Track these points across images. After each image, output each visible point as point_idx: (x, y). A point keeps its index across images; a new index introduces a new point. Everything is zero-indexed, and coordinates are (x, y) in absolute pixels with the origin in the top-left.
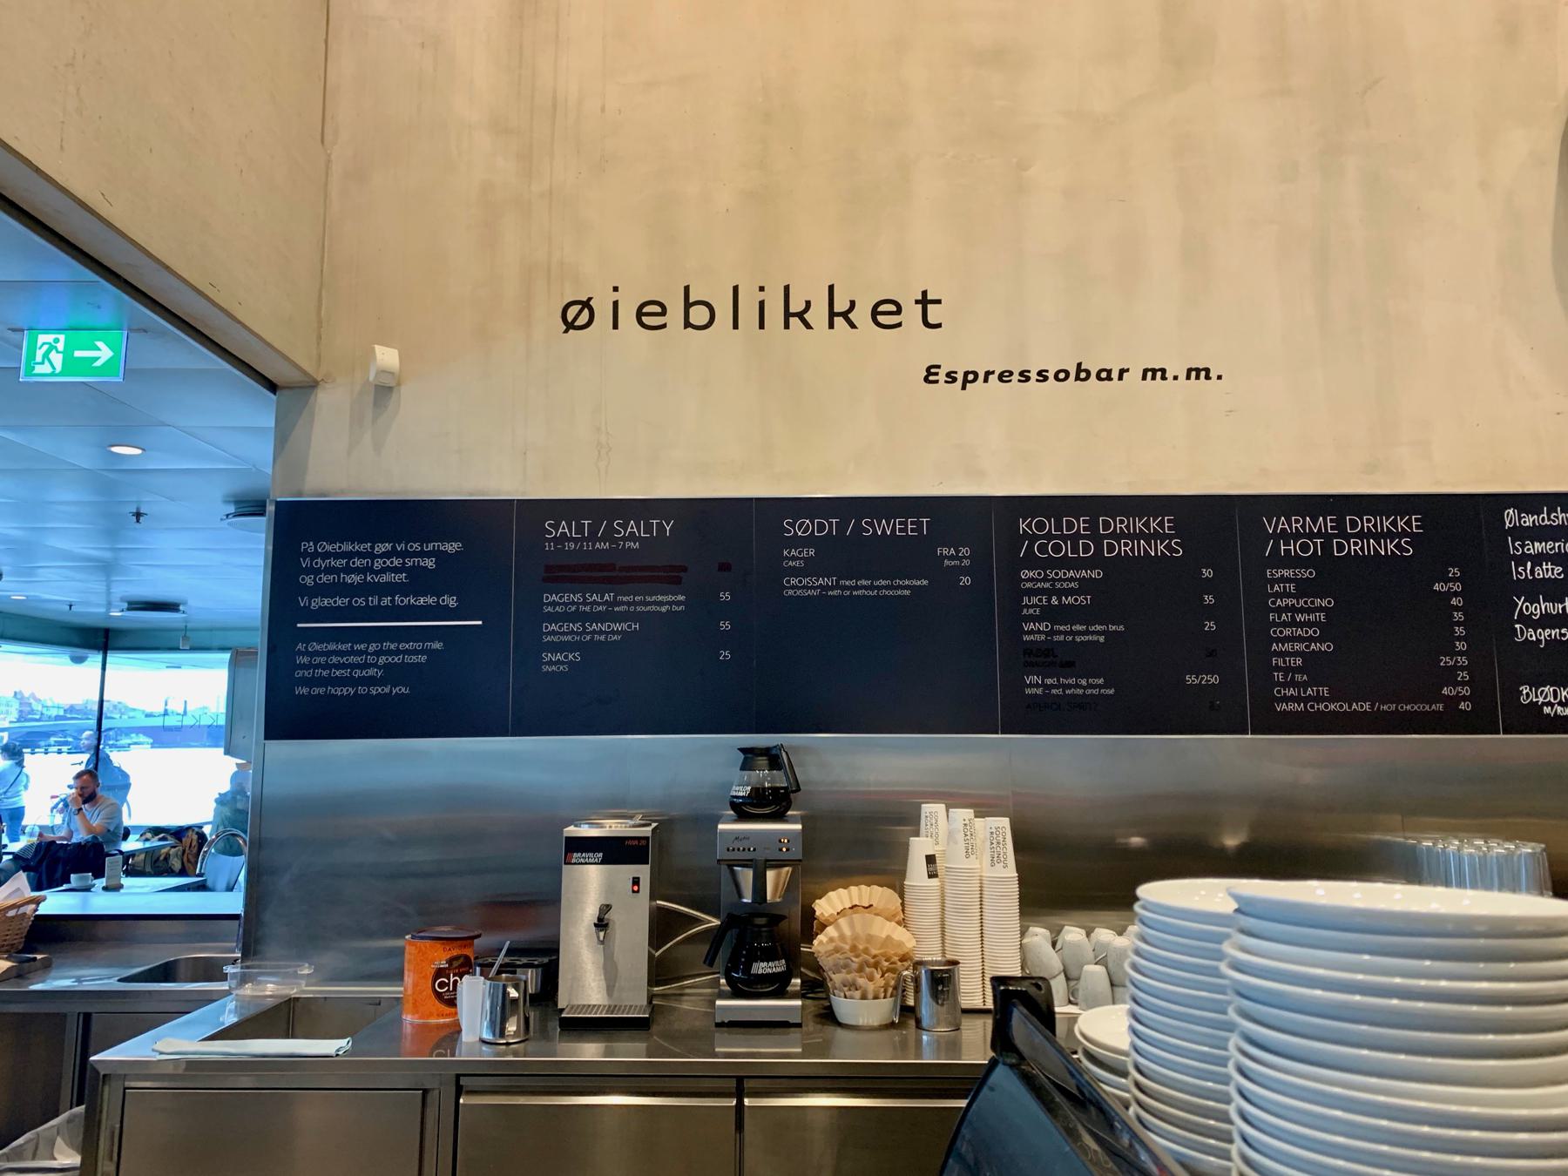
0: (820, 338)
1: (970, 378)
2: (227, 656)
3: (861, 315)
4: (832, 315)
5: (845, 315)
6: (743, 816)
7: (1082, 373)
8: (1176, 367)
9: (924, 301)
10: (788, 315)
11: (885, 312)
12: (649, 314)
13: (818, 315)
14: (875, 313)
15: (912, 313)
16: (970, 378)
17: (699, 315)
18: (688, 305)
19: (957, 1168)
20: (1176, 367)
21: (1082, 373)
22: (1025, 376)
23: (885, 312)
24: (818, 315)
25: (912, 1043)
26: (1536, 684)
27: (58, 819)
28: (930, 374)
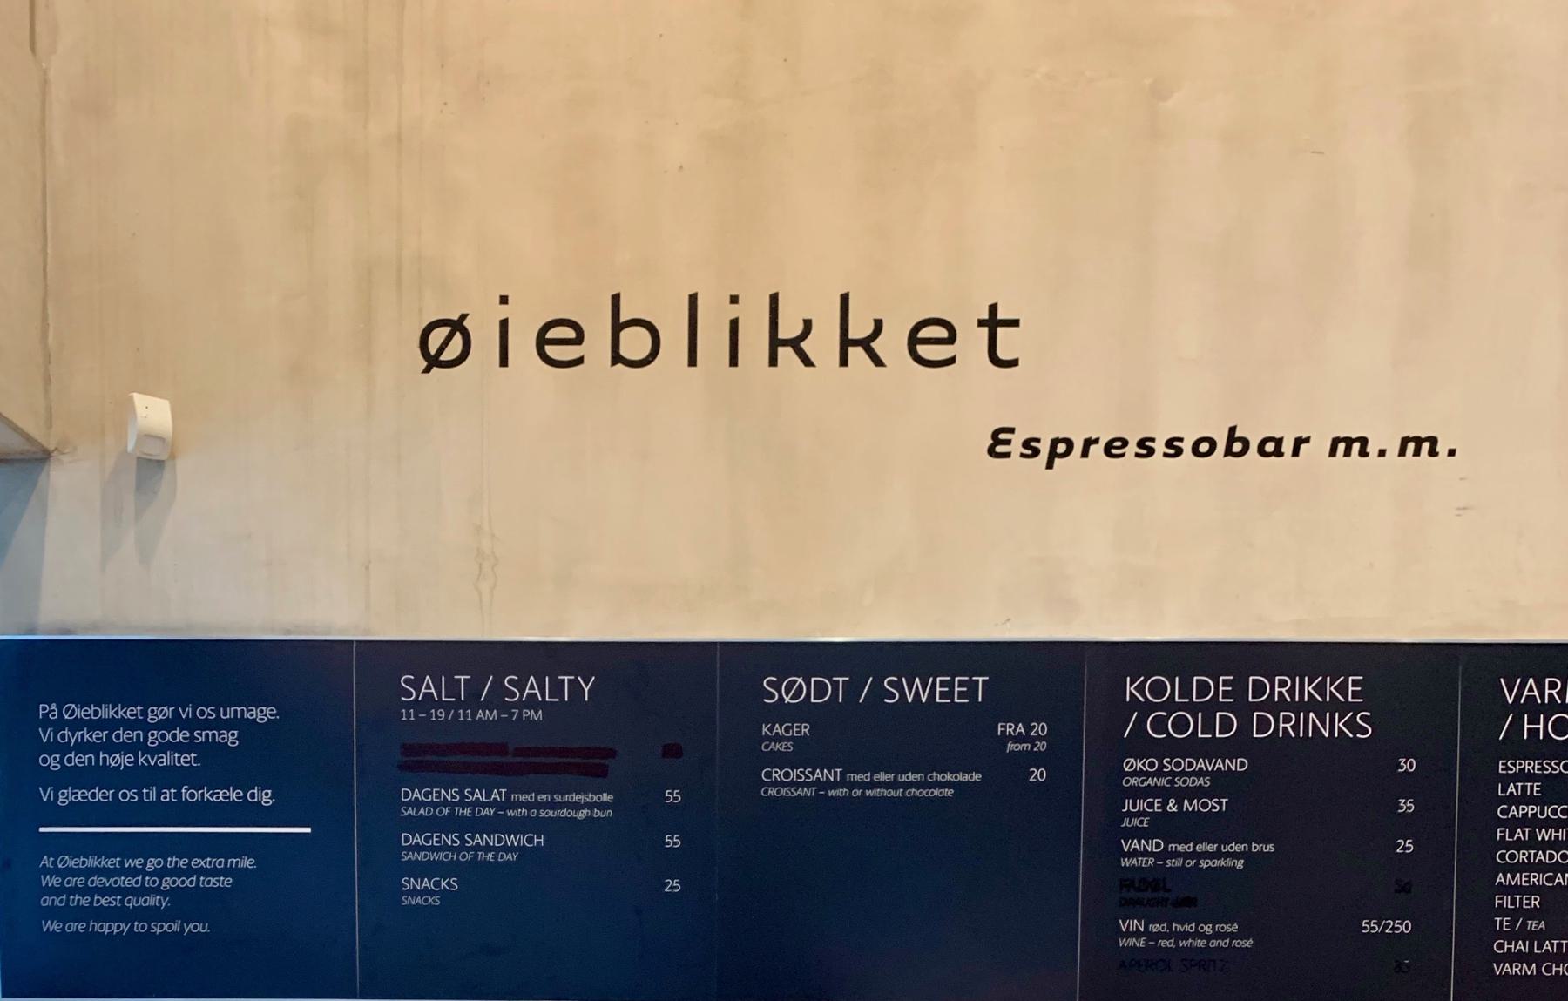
0: (824, 387)
1: (1060, 449)
3: (892, 344)
4: (846, 343)
5: (866, 344)
8: (1384, 436)
9: (992, 322)
10: (775, 342)
11: (929, 340)
12: (557, 340)
13: (823, 344)
14: (914, 341)
15: (973, 340)
16: (1060, 449)
17: (635, 343)
18: (618, 327)
20: (1384, 436)
21: (1235, 445)
23: (929, 340)
24: (823, 344)
28: (998, 443)
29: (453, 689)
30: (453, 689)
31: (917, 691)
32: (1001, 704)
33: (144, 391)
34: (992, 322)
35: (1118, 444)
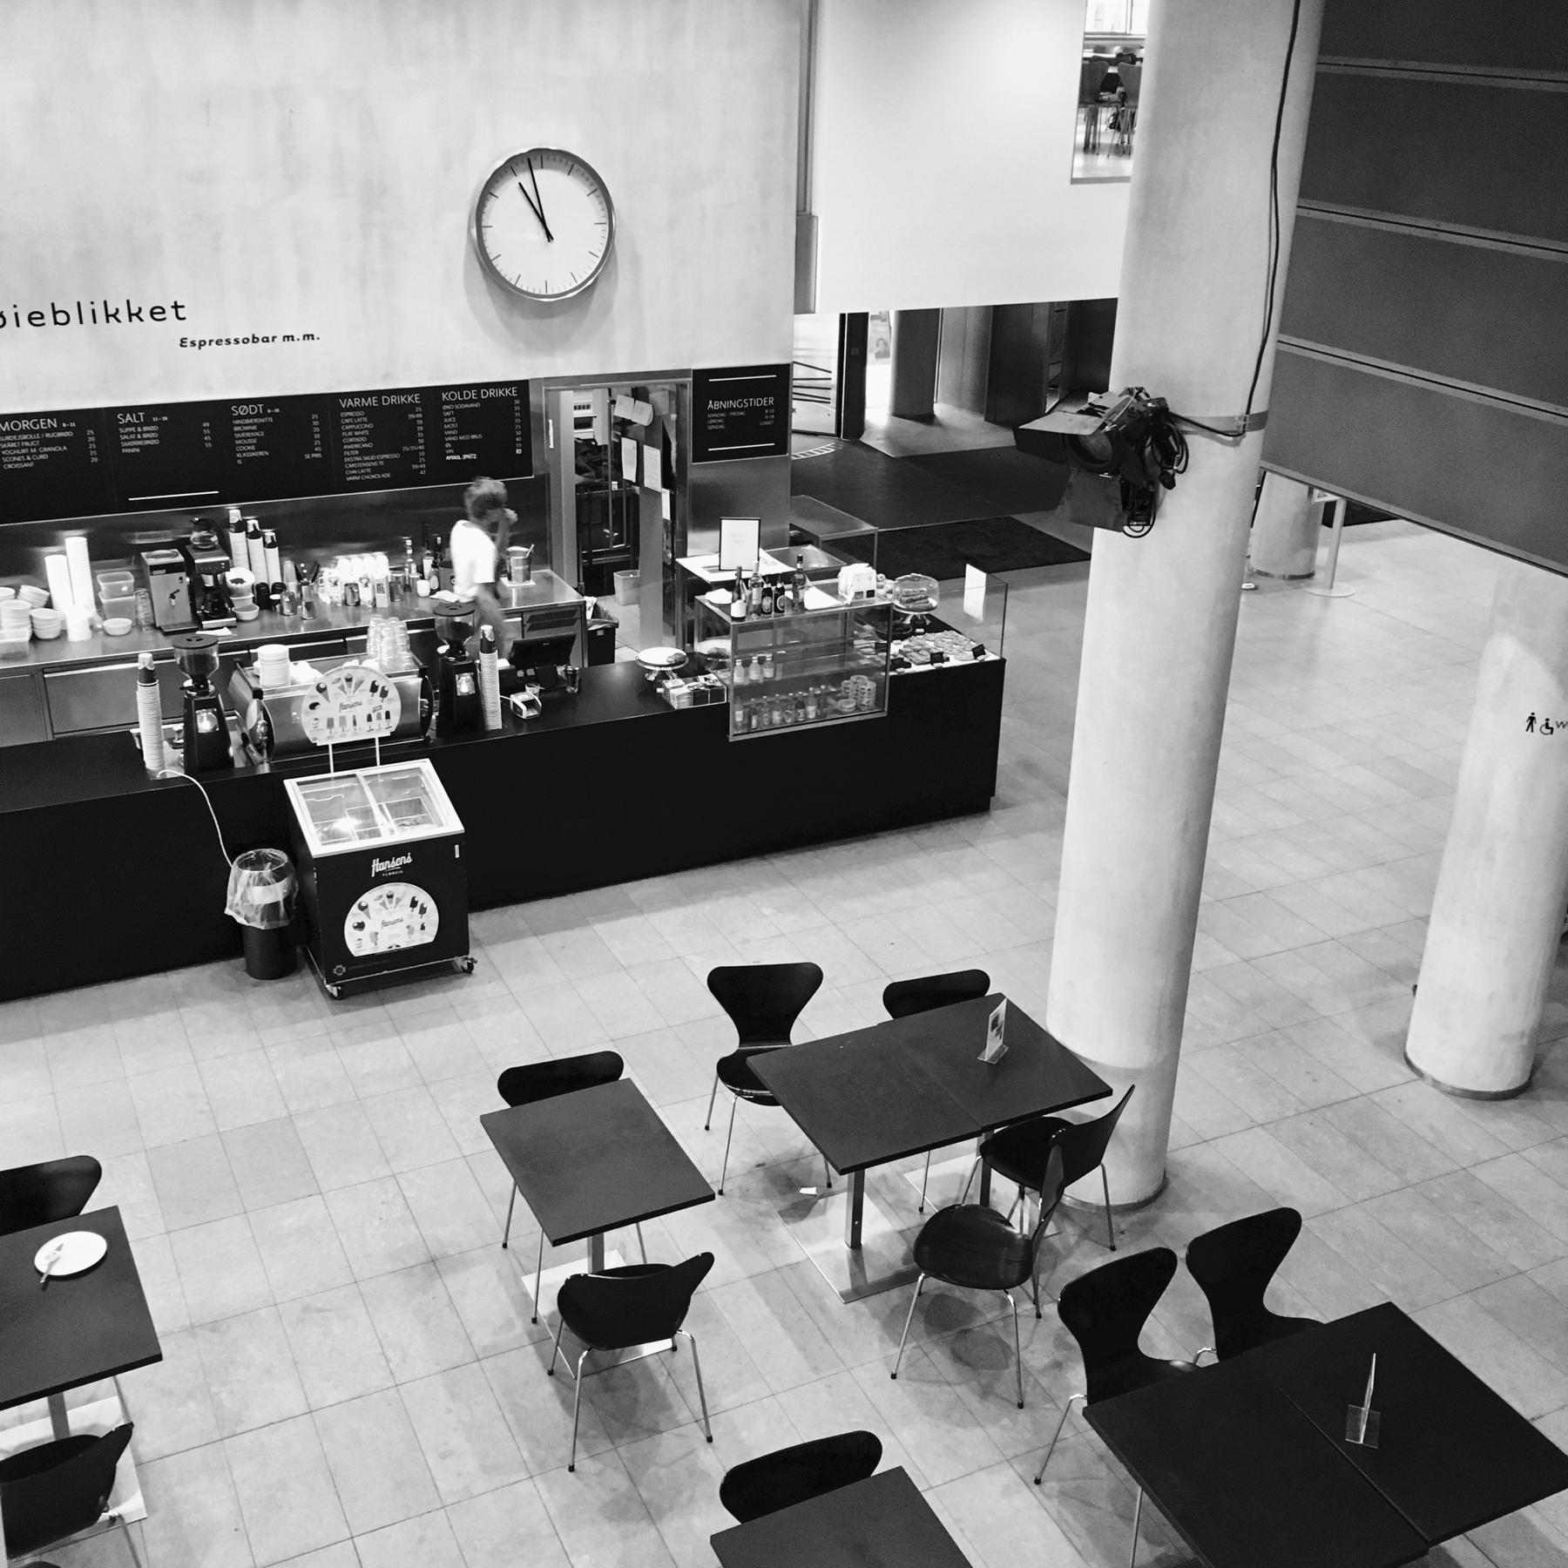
0: (125, 326)
1: (202, 344)
2: (864, 439)
3: (145, 314)
4: (130, 315)
5: (137, 315)
6: (718, 655)
7: (255, 339)
8: (298, 335)
9: (176, 307)
10: (108, 316)
11: (157, 313)
12: (35, 318)
13: (123, 315)
14: (152, 313)
15: (170, 313)
16: (202, 344)
17: (61, 318)
18: (55, 313)
19: (1399, 1079)
20: (298, 335)
21: (255, 339)
22: (237, 341)
23: (157, 313)
24: (123, 315)
25: (952, 374)
26: (231, 761)
27: (284, 882)
28: (183, 342)
29: (138, 418)
30: (138, 418)
31: (491, 393)
32: (80, 433)
33: (973, 564)
34: (176, 307)
35: (389, 920)
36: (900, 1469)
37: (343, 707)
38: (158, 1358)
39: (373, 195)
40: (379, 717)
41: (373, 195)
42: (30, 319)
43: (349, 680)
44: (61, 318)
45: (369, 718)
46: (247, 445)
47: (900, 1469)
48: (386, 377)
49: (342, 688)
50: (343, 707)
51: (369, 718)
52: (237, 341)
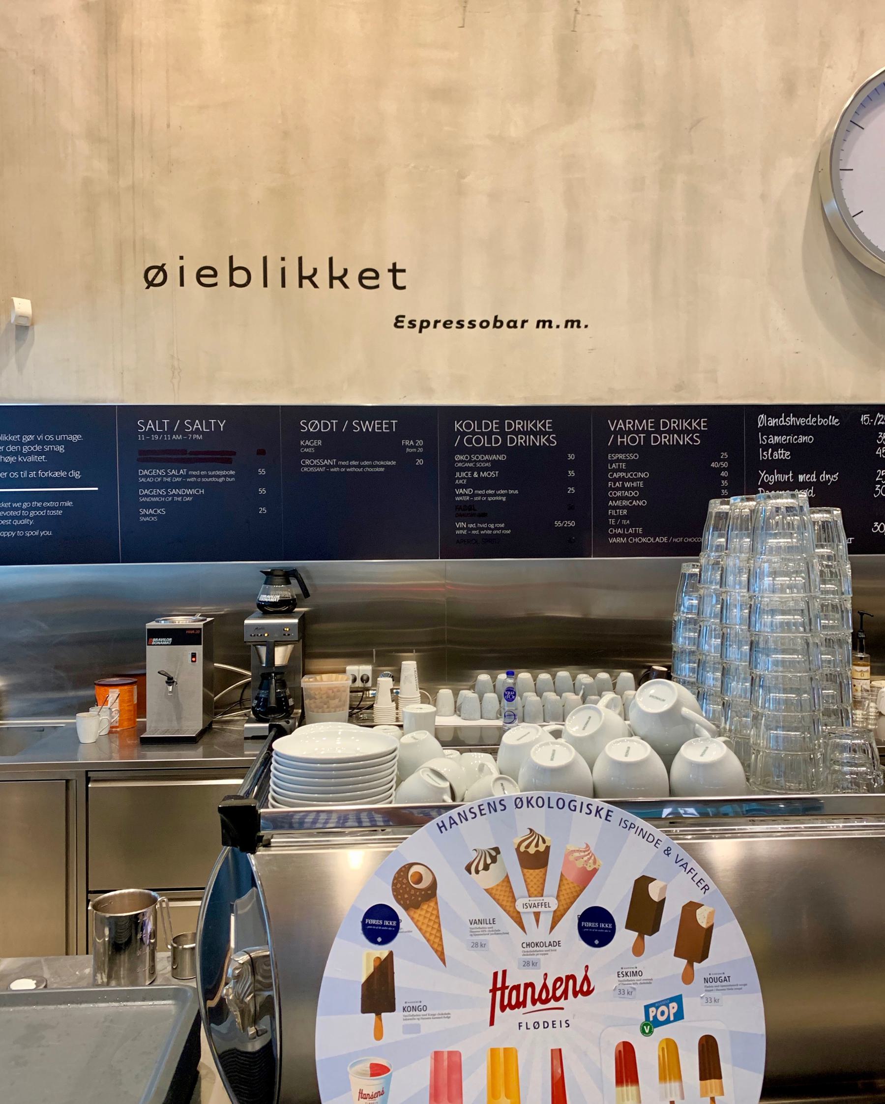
0: (323, 295)
1: (424, 325)
3: (352, 279)
4: (332, 278)
5: (340, 279)
7: (498, 323)
8: (558, 319)
9: (394, 270)
10: (301, 278)
12: (205, 275)
13: (322, 278)
14: (361, 278)
15: (386, 278)
16: (424, 325)
17: (240, 277)
18: (232, 270)
20: (558, 319)
21: (498, 323)
24: (322, 278)
28: (398, 322)
36: (683, 1018)
37: (506, 996)
38: (560, 1050)
39: (680, 126)
40: (670, 1069)
41: (680, 126)
42: (199, 276)
43: (535, 860)
44: (240, 277)
45: (626, 1068)
46: (472, 473)
47: (683, 1018)
48: (679, 388)
49: (504, 895)
50: (506, 996)
51: (626, 1068)
52: (472, 324)
